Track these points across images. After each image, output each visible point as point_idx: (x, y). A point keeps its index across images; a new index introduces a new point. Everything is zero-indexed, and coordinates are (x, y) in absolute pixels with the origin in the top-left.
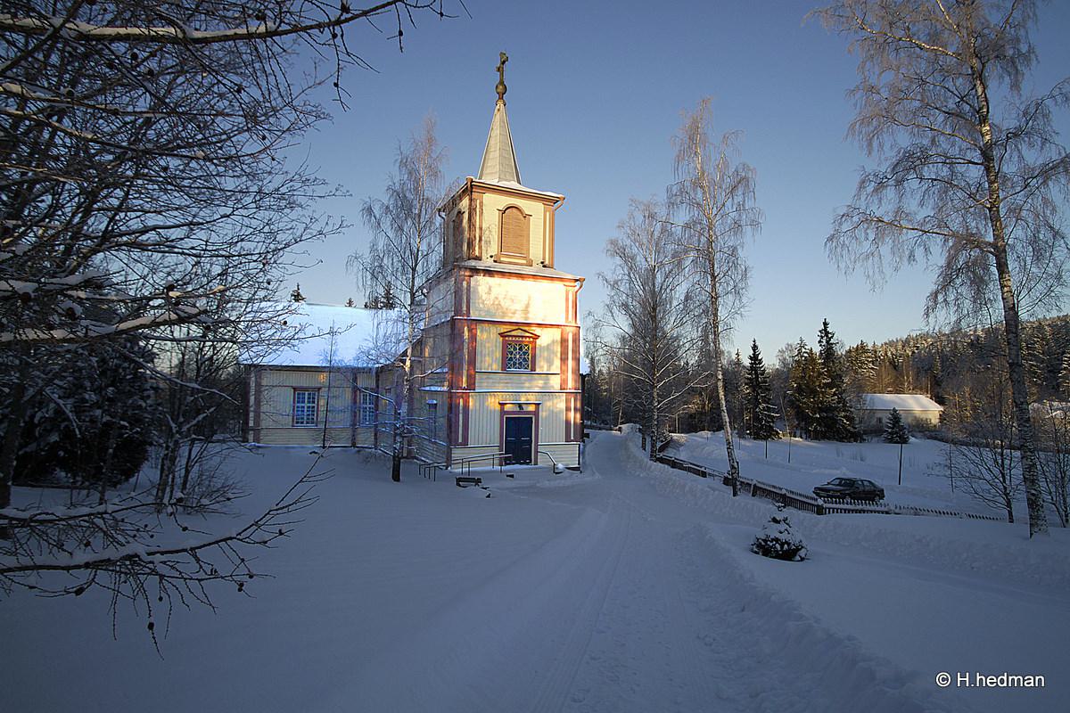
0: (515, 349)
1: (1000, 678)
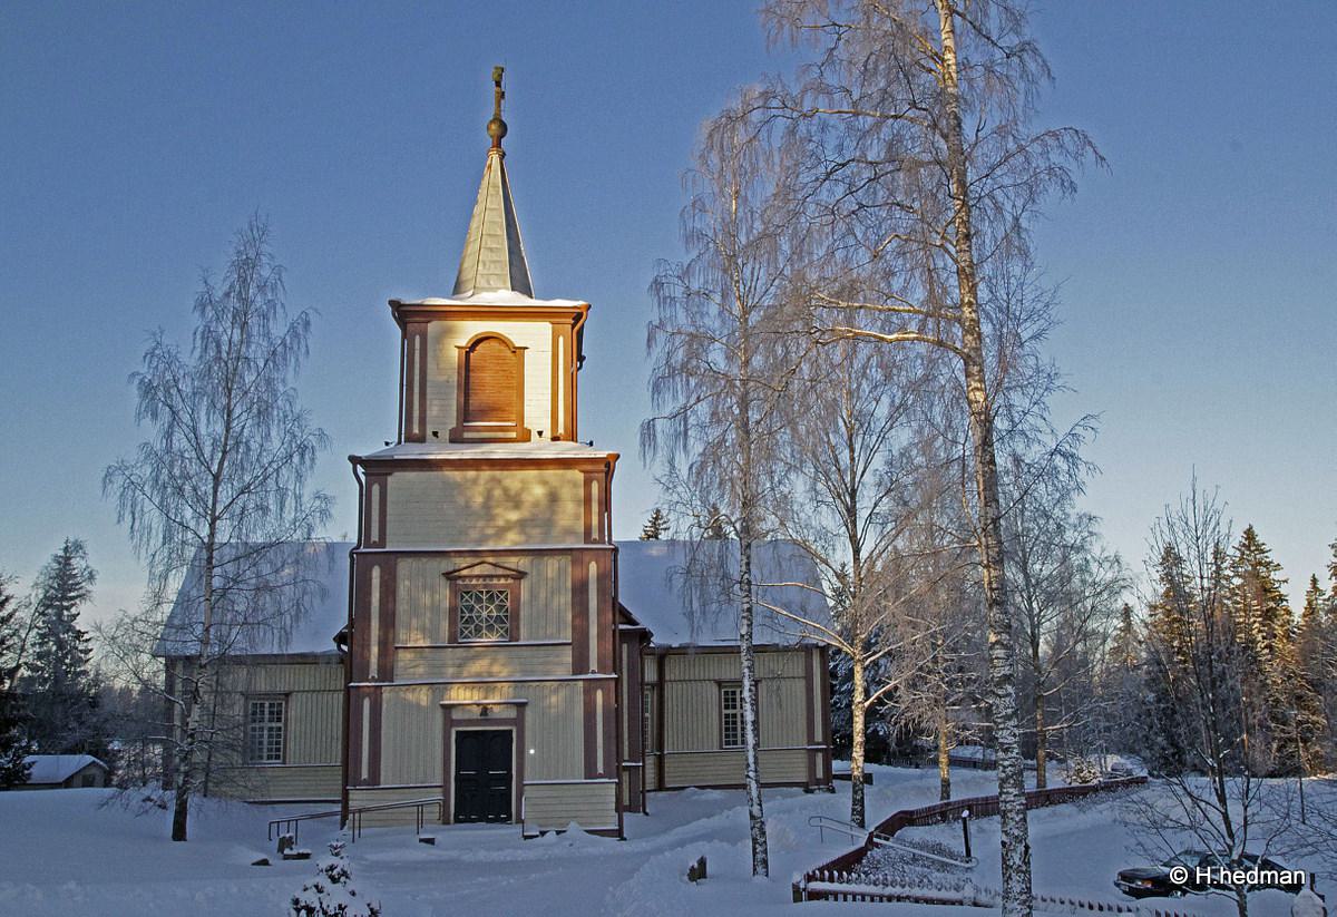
0: (479, 600)
1: (1249, 873)
